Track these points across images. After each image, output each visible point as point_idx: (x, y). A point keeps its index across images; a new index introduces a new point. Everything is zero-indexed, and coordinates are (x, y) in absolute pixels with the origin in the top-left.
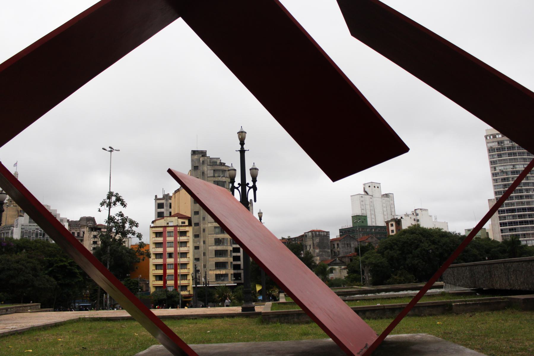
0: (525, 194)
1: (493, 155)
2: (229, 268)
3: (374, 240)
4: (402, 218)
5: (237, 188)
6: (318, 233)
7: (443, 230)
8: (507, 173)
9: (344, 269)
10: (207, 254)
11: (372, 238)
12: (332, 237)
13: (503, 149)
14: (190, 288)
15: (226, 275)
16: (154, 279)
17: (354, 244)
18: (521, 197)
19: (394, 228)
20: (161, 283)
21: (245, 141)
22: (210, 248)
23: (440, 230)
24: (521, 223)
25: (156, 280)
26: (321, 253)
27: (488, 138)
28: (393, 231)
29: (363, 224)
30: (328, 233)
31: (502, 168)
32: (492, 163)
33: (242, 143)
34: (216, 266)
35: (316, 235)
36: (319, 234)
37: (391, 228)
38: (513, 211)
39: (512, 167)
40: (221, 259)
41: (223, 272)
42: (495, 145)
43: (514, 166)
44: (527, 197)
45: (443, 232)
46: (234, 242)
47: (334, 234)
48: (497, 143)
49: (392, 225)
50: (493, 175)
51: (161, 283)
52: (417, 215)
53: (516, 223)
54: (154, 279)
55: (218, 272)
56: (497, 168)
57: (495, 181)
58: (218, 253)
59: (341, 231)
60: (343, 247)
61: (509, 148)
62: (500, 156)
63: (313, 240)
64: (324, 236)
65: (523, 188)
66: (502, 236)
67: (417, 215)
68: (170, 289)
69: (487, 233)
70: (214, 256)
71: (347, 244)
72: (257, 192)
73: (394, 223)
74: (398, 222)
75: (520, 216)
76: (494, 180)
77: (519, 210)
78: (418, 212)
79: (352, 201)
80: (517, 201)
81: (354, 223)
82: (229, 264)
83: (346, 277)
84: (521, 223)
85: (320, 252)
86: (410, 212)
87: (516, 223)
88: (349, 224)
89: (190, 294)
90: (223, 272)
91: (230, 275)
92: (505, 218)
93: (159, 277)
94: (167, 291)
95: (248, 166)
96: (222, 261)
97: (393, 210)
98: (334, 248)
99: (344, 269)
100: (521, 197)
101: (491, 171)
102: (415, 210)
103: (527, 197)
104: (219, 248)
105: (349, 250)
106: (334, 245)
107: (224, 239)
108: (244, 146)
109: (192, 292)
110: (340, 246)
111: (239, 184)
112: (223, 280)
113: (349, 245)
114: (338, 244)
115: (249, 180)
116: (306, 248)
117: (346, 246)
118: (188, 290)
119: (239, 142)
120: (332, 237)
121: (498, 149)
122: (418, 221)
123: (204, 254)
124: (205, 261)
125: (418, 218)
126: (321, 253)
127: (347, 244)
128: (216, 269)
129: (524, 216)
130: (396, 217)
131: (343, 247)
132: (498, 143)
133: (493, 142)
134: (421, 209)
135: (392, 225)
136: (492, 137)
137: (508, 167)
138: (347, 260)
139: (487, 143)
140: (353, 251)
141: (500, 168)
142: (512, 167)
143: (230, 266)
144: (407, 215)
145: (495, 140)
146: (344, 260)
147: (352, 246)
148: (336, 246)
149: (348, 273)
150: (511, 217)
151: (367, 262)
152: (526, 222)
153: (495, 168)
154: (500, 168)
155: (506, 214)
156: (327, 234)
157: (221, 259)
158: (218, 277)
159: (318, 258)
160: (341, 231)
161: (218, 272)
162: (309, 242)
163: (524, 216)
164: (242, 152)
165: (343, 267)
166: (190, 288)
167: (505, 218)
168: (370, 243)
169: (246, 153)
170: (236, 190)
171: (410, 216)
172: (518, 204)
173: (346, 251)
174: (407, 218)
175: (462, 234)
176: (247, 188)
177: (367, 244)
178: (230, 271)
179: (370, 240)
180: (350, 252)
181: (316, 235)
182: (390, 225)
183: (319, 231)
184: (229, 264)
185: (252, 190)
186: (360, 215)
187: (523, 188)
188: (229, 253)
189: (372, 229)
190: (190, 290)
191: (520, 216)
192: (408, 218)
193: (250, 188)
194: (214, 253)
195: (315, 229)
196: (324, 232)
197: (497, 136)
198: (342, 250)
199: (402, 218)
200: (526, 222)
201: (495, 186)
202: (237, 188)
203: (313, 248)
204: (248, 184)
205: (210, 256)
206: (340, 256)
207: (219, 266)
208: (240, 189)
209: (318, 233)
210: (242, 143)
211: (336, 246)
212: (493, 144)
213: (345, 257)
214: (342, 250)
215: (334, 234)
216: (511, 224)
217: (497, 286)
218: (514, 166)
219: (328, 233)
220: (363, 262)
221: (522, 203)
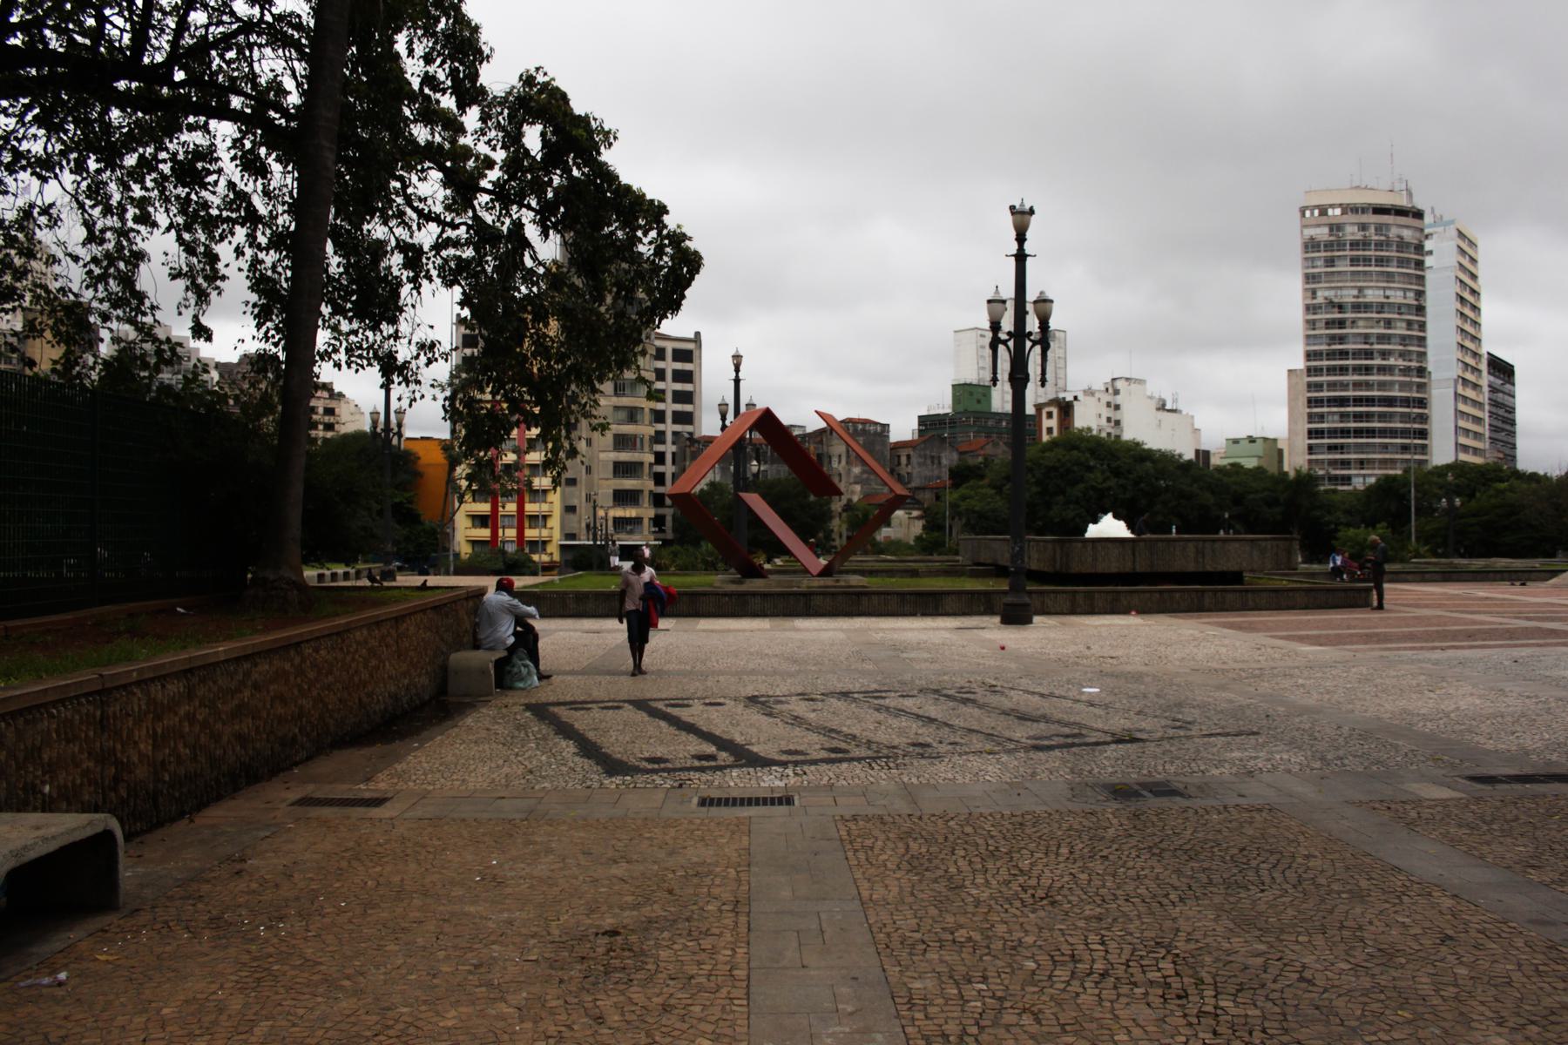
0: (1377, 362)
1: (1313, 259)
5: (1005, 342)
8: (1341, 307)
9: (918, 518)
10: (594, 469)
12: (895, 437)
13: (1340, 245)
14: (553, 548)
15: (638, 521)
16: (469, 523)
17: (949, 458)
18: (1368, 370)
19: (1053, 423)
20: (485, 533)
21: (1028, 235)
22: (602, 456)
24: (1358, 433)
27: (1308, 213)
28: (1050, 430)
29: (978, 408)
30: (885, 427)
31: (1330, 294)
32: (1309, 278)
35: (855, 429)
37: (1046, 423)
38: (1342, 402)
39: (1355, 292)
41: (631, 512)
42: (1322, 233)
43: (1360, 289)
44: (1382, 370)
46: (812, 448)
47: (903, 429)
48: (1326, 230)
49: (1050, 415)
50: (1309, 309)
51: (485, 533)
52: (1117, 392)
53: (1345, 433)
55: (620, 512)
56: (1319, 294)
57: (1311, 324)
58: (622, 469)
59: (923, 420)
60: (920, 464)
61: (1355, 245)
62: (1330, 262)
64: (876, 433)
65: (1376, 347)
66: (1310, 461)
67: (1117, 392)
69: (1280, 452)
72: (1049, 353)
73: (1055, 411)
74: (1066, 409)
75: (1358, 417)
76: (1307, 322)
77: (1358, 401)
78: (1119, 385)
80: (1356, 378)
83: (918, 539)
84: (1358, 433)
87: (1345, 433)
88: (943, 404)
90: (631, 512)
91: (646, 521)
92: (1321, 417)
93: (480, 520)
94: (504, 552)
95: (1031, 296)
99: (918, 518)
100: (1368, 370)
101: (1305, 298)
103: (1382, 370)
109: (557, 557)
110: (914, 460)
111: (1009, 333)
112: (631, 532)
113: (936, 460)
114: (909, 457)
115: (1033, 324)
119: (1013, 234)
120: (895, 437)
121: (1329, 246)
122: (1117, 407)
123: (589, 470)
124: (590, 485)
125: (1119, 399)
129: (1368, 416)
130: (1061, 395)
131: (920, 464)
132: (1331, 230)
133: (1318, 226)
134: (1127, 379)
135: (1050, 415)
136: (1316, 212)
137: (1345, 292)
138: (927, 497)
139: (1304, 226)
140: (946, 476)
141: (1327, 293)
142: (1355, 292)
144: (1090, 392)
145: (1324, 220)
146: (920, 496)
147: (944, 461)
148: (904, 460)
149: (924, 528)
150: (1336, 418)
151: (963, 506)
152: (1371, 433)
153: (1314, 292)
154: (1327, 293)
155: (1325, 410)
157: (629, 484)
158: (620, 523)
159: (858, 488)
160: (923, 420)
161: (620, 512)
162: (838, 448)
163: (1368, 416)
165: (915, 513)
166: (553, 548)
167: (1321, 417)
169: (1029, 262)
170: (1001, 348)
172: (1357, 385)
173: (928, 473)
174: (1089, 399)
176: (1028, 344)
177: (980, 459)
178: (647, 512)
179: (989, 450)
181: (855, 429)
182: (1044, 415)
183: (866, 422)
184: (646, 494)
185: (1038, 349)
187: (1376, 347)
188: (646, 467)
189: (1000, 421)
191: (1358, 417)
193: (1035, 343)
196: (876, 423)
197: (1330, 212)
198: (918, 472)
200: (1371, 433)
201: (1308, 337)
202: (1005, 342)
204: (1030, 333)
206: (913, 485)
207: (622, 498)
208: (1011, 344)
212: (1318, 231)
213: (923, 489)
215: (903, 429)
216: (1333, 433)
217: (1076, 568)
218: (1360, 289)
219: (885, 427)
220: (954, 506)
221: (1368, 386)
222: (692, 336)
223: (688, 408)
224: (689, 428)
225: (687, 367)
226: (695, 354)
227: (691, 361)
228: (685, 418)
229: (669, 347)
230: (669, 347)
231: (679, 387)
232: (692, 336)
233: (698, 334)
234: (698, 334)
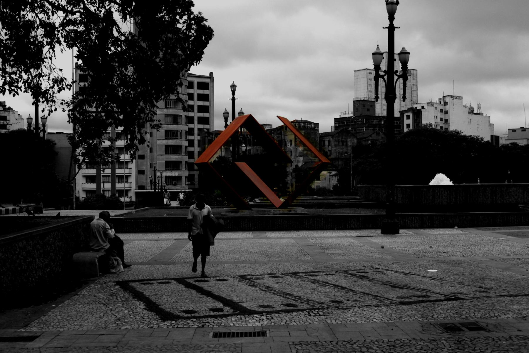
2: (184, 170)
3: (380, 138)
4: (423, 107)
6: (302, 125)
7: (462, 134)
9: (335, 175)
11: (378, 134)
12: (321, 130)
14: (132, 194)
15: (179, 178)
19: (410, 122)
20: (93, 186)
22: (159, 142)
23: (458, 133)
25: (87, 182)
26: (305, 152)
28: (408, 126)
29: (368, 113)
30: (317, 125)
33: (233, 93)
34: (166, 167)
35: (300, 126)
36: (304, 126)
37: (406, 122)
40: (174, 158)
41: (175, 174)
45: (462, 136)
47: (326, 125)
49: (408, 117)
51: (93, 186)
52: (446, 104)
54: (84, 181)
55: (169, 174)
63: (228, 315)
64: (311, 128)
67: (446, 104)
68: (108, 194)
70: (164, 154)
71: (343, 142)
73: (411, 115)
78: (448, 100)
79: (356, 78)
81: (356, 109)
82: (184, 163)
83: (335, 187)
85: (304, 150)
86: (436, 100)
89: (131, 201)
90: (175, 174)
91: (184, 179)
96: (174, 160)
97: (414, 94)
98: (324, 145)
99: (335, 175)
102: (444, 97)
104: (171, 142)
105: (345, 150)
106: (324, 141)
107: (177, 131)
108: (235, 96)
109: (134, 199)
110: (333, 143)
112: (175, 185)
114: (329, 141)
116: (286, 145)
117: (341, 144)
118: (129, 195)
119: (231, 92)
120: (321, 130)
123: (151, 150)
124: (152, 159)
125: (447, 108)
126: (305, 152)
127: (343, 142)
128: (166, 170)
134: (452, 96)
135: (408, 117)
143: (184, 166)
144: (431, 104)
147: (349, 144)
148: (327, 143)
156: (315, 127)
157: (174, 158)
159: (301, 159)
161: (169, 174)
164: (233, 100)
165: (333, 173)
166: (132, 194)
168: (372, 141)
171: (435, 106)
173: (341, 150)
174: (431, 108)
175: (486, 140)
179: (374, 137)
180: (346, 153)
181: (300, 126)
182: (405, 117)
184: (184, 163)
186: (366, 99)
190: (132, 196)
192: (432, 109)
194: (164, 148)
195: (299, 118)
196: (311, 123)
199: (423, 107)
203: (295, 145)
205: (158, 153)
209: (302, 125)
210: (233, 93)
211: (327, 143)
214: (334, 149)
215: (326, 125)
219: (317, 125)
222: (208, 75)
223: (206, 115)
224: (207, 126)
225: (206, 92)
226: (210, 85)
227: (208, 89)
228: (205, 121)
229: (196, 81)
230: (196, 81)
231: (201, 103)
232: (208, 75)
233: (211, 74)
234: (211, 74)
